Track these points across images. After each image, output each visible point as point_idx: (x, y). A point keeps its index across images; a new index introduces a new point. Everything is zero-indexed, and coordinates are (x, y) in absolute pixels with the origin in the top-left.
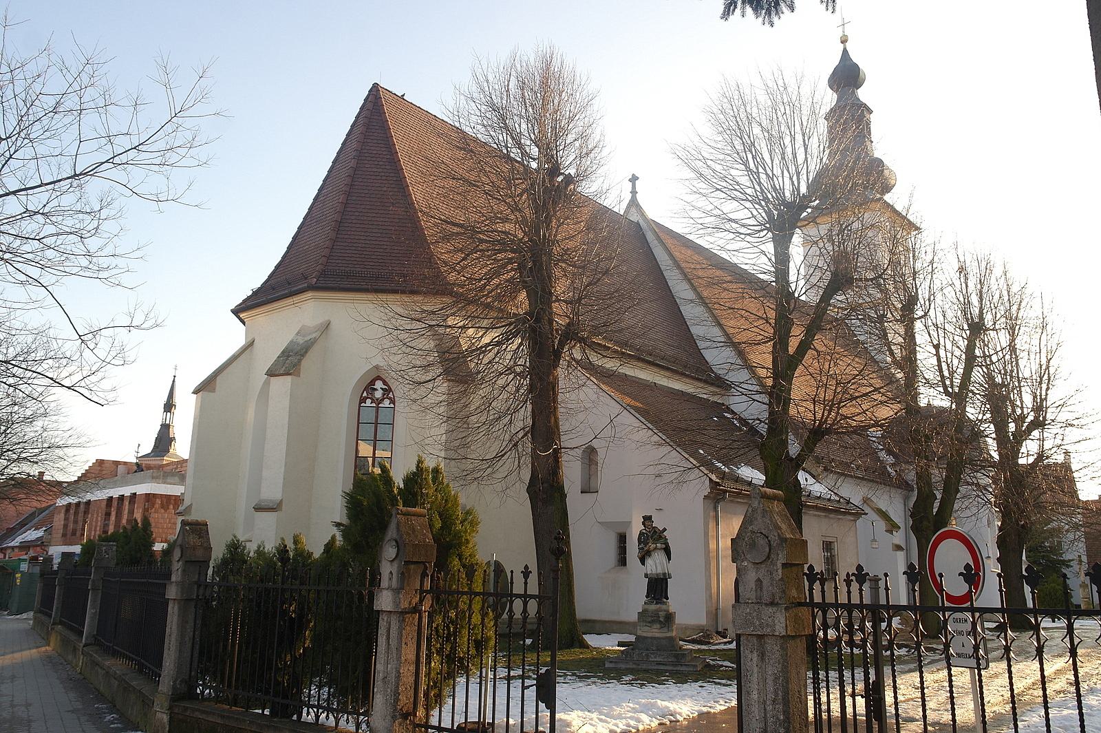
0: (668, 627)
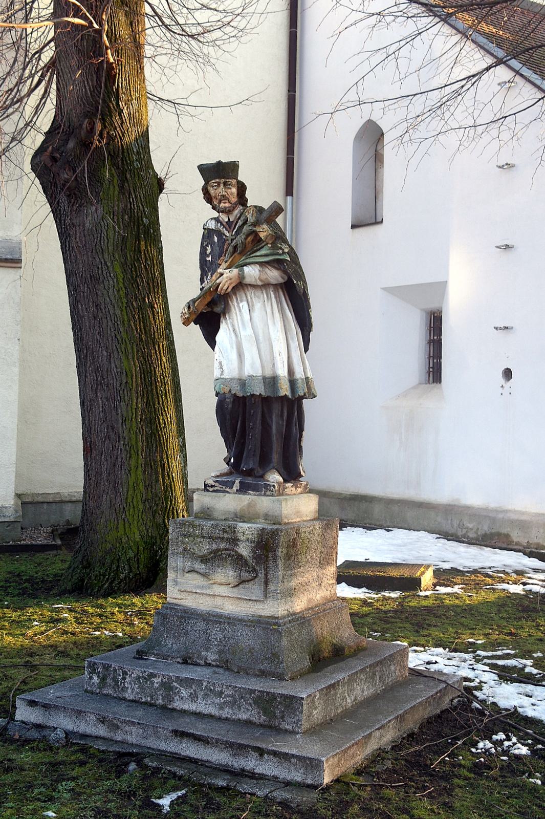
0: (266, 583)
